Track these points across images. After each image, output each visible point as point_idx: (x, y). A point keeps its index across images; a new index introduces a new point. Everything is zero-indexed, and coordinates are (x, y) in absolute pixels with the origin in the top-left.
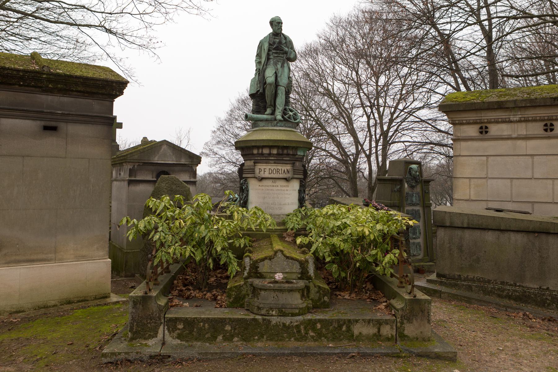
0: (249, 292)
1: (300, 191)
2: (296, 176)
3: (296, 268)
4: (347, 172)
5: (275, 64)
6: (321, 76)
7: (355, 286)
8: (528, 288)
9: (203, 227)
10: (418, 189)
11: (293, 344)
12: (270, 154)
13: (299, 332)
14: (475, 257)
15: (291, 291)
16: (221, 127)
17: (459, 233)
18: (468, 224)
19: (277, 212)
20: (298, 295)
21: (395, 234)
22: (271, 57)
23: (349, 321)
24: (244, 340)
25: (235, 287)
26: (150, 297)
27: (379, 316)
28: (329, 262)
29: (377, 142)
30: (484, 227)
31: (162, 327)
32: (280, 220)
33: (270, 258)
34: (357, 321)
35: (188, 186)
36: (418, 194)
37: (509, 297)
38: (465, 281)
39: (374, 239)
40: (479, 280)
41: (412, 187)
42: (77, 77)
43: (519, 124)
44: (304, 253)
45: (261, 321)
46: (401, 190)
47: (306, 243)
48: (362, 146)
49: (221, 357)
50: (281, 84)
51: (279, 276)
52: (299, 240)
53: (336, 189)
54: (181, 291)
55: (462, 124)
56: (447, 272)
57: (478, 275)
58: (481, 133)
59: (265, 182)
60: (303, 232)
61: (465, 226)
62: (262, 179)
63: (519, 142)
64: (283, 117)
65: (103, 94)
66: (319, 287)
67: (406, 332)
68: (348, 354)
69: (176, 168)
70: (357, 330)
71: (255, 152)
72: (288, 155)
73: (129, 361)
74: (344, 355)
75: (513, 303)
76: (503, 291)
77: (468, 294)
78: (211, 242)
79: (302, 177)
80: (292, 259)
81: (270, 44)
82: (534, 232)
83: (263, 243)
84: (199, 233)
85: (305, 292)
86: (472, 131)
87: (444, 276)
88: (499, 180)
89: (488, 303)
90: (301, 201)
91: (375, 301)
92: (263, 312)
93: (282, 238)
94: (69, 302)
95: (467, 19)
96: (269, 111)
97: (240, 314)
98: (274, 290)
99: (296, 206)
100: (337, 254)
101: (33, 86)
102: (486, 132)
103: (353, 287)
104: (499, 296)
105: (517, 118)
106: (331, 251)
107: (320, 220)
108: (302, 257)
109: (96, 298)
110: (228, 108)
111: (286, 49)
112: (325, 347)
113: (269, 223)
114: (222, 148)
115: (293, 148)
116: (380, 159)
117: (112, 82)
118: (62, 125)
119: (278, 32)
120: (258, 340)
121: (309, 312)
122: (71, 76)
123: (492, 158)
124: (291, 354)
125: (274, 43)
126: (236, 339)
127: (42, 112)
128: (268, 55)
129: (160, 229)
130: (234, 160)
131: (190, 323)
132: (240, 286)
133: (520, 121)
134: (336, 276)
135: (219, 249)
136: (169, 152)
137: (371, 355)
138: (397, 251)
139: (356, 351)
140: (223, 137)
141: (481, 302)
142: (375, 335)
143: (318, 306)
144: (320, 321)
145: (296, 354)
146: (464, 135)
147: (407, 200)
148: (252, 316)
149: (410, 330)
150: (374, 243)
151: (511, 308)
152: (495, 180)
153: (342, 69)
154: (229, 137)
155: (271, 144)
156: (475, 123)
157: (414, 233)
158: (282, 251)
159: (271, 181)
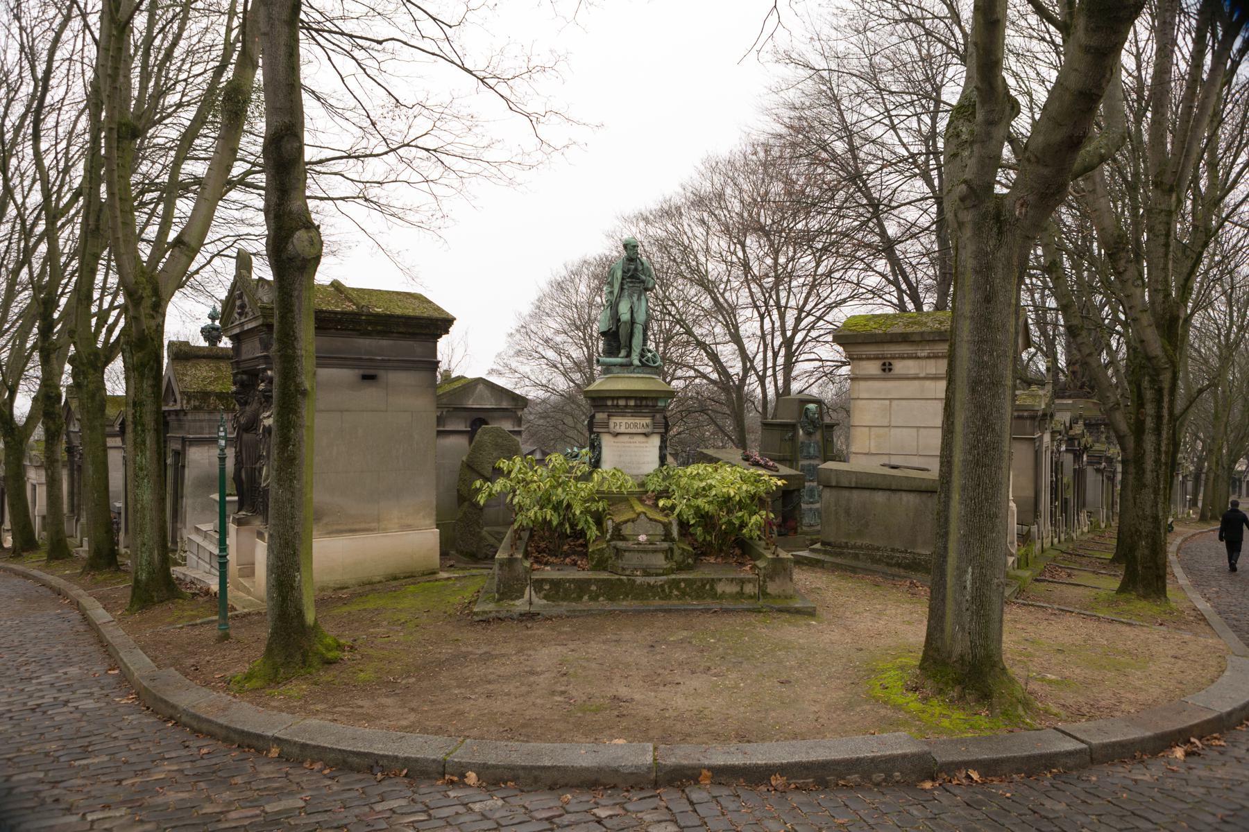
0: (612, 555)
1: (661, 448)
2: (656, 430)
3: (660, 530)
4: (729, 402)
5: (631, 296)
6: (686, 250)
7: (721, 551)
8: (919, 554)
9: (560, 490)
10: (818, 436)
11: (657, 602)
12: (626, 406)
13: (663, 591)
14: (863, 522)
15: (655, 551)
16: (522, 327)
17: (846, 493)
18: (856, 483)
19: (635, 472)
20: (661, 556)
21: (764, 495)
22: (625, 287)
23: (713, 580)
24: (610, 599)
25: (598, 550)
26: (516, 559)
27: (742, 575)
28: (693, 525)
29: (775, 355)
30: (873, 486)
31: (528, 588)
32: (640, 481)
33: (633, 521)
34: (720, 580)
35: (514, 437)
36: (817, 443)
37: (899, 565)
38: (852, 549)
39: (740, 500)
40: (867, 548)
41: (809, 434)
42: (398, 317)
43: (928, 361)
44: (667, 515)
45: (626, 581)
46: (794, 438)
47: (669, 505)
48: (752, 362)
49: (589, 613)
50: (637, 321)
51: (642, 538)
52: (661, 503)
53: (712, 428)
54: (536, 557)
55: (861, 359)
56: (832, 540)
57: (867, 542)
58: (884, 370)
59: (621, 438)
60: (666, 493)
61: (853, 485)
62: (618, 434)
63: (928, 383)
64: (640, 361)
65: (426, 335)
66: (683, 549)
67: (768, 591)
68: (710, 609)
69: (496, 414)
70: (720, 588)
71: (609, 403)
72: (647, 406)
73: (500, 619)
74: (707, 611)
75: (902, 572)
76: (892, 559)
77: (854, 563)
78: (569, 506)
79: (663, 430)
80: (656, 521)
81: (624, 272)
82: (927, 492)
83: (622, 506)
84: (557, 495)
85: (669, 553)
86: (873, 368)
87: (829, 544)
88: (904, 430)
89: (874, 572)
90: (663, 459)
91: (742, 564)
92: (628, 572)
93: (642, 501)
94: (395, 578)
95: (818, 295)
96: (623, 353)
97: (604, 575)
98: (639, 551)
99: (656, 465)
100: (702, 516)
101: (351, 330)
102: (890, 370)
103: (719, 552)
104: (888, 564)
105: (925, 353)
106: (695, 513)
107: (684, 481)
108: (665, 520)
109: (423, 574)
110: (534, 296)
111: (643, 277)
112: (689, 604)
113: (629, 484)
114: (525, 361)
115: (653, 398)
116: (780, 383)
117: (437, 320)
118: (381, 373)
119: (634, 257)
120: (623, 599)
121: (673, 573)
122: (391, 316)
123: (896, 402)
124: (656, 610)
125: (629, 270)
126: (601, 598)
127: (361, 359)
128: (622, 284)
129: (518, 492)
130: (544, 382)
131: (556, 584)
132: (603, 549)
133: (928, 357)
134: (700, 540)
135: (578, 512)
136: (487, 393)
137: (732, 611)
138: (763, 513)
139: (719, 607)
140: (527, 344)
141: (865, 570)
142: (737, 593)
143: (681, 568)
144: (684, 580)
145: (661, 611)
146: (862, 372)
147: (802, 452)
148: (617, 577)
149: (772, 588)
150: (741, 505)
151: (899, 576)
152: (900, 429)
153: (719, 244)
154: (536, 344)
155: (627, 395)
156: (876, 358)
157: (812, 496)
158: (645, 513)
159: (628, 436)
